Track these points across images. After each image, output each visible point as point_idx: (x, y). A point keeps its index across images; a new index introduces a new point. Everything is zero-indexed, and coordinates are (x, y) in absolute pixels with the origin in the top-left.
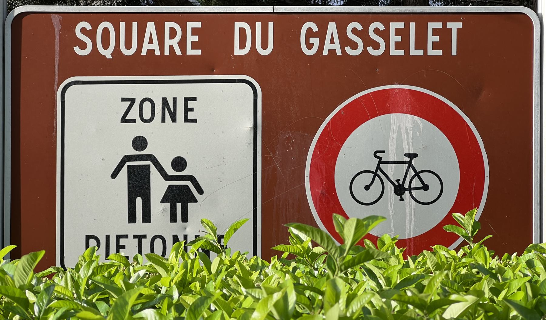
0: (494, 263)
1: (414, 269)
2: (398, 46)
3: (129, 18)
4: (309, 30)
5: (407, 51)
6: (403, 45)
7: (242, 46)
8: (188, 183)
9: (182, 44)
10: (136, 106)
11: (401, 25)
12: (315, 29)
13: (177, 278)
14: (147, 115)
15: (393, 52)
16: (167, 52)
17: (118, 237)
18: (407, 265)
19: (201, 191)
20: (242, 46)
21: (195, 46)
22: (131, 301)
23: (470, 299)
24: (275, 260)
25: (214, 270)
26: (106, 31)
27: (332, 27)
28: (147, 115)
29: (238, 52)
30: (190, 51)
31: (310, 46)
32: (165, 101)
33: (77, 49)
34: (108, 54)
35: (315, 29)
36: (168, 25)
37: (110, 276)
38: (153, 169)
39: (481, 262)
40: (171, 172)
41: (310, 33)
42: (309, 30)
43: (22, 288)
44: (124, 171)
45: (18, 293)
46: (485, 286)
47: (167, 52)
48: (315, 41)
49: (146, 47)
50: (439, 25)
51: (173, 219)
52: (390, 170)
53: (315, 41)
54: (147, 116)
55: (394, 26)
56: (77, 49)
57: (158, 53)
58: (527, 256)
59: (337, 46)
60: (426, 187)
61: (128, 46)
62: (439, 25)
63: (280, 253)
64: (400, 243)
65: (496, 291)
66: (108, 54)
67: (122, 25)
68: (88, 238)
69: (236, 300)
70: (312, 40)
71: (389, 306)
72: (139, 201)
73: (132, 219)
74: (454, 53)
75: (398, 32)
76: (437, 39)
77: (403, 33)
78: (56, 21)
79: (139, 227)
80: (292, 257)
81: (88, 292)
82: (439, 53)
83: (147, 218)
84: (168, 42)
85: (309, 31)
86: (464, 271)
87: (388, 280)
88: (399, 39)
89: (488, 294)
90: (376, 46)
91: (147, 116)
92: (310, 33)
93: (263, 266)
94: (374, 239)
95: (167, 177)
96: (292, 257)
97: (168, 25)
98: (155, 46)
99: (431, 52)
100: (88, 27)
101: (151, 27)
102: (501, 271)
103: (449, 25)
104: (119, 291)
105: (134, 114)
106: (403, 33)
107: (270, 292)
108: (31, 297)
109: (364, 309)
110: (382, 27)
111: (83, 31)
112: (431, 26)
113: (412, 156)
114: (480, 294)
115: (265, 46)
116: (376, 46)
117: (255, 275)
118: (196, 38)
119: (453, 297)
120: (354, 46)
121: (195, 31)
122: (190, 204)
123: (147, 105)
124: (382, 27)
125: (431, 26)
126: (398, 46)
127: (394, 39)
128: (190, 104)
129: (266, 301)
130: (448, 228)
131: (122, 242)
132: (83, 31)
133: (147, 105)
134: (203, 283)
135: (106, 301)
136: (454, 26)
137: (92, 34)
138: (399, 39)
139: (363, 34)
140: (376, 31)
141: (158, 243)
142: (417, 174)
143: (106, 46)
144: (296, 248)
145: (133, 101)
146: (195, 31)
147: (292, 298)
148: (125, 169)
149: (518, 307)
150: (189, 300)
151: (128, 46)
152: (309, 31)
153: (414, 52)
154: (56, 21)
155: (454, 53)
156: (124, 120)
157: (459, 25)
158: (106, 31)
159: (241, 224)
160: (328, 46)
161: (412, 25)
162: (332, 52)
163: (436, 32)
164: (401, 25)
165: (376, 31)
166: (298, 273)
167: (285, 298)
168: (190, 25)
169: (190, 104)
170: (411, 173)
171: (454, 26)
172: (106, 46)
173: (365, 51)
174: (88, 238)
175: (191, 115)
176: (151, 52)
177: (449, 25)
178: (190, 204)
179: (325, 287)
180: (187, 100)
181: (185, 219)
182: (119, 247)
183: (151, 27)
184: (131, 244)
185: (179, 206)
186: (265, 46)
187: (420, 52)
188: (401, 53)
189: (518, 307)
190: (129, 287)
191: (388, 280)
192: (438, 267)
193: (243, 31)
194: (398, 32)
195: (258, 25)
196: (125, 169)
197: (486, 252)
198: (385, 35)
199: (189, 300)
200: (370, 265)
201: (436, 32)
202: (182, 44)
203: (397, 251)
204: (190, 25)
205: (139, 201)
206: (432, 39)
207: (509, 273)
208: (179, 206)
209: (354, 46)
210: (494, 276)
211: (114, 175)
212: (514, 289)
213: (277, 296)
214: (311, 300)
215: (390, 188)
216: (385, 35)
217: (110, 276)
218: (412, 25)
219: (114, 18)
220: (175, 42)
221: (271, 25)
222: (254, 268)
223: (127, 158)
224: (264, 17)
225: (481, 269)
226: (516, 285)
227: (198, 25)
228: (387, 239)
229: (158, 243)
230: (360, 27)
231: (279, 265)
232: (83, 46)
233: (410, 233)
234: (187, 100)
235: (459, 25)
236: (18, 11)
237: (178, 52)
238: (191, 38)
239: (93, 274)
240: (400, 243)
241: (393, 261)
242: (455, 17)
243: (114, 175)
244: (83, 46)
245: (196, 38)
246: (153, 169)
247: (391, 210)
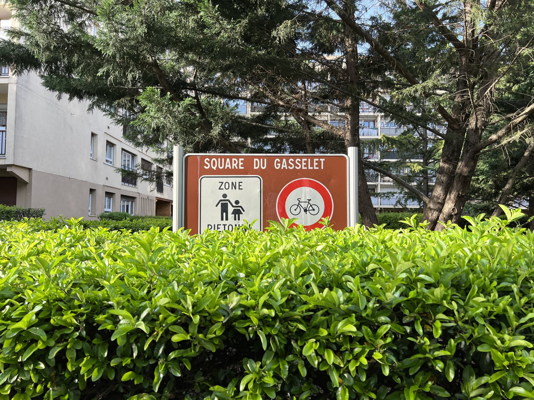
0: (334, 233)
1: (309, 235)
2: (305, 166)
3: (221, 157)
4: (277, 161)
5: (308, 168)
6: (306, 166)
7: (257, 166)
8: (240, 208)
9: (238, 165)
10: (224, 184)
11: (306, 160)
12: (279, 161)
13: (234, 238)
14: (227, 187)
15: (303, 168)
16: (233, 168)
17: (218, 225)
18: (306, 234)
19: (244, 211)
20: (257, 166)
21: (242, 166)
22: (218, 245)
23: (324, 244)
24: (266, 232)
25: (246, 235)
26: (214, 161)
27: (284, 160)
28: (227, 187)
29: (255, 168)
30: (240, 168)
31: (277, 166)
32: (232, 183)
33: (205, 167)
34: (215, 168)
35: (279, 161)
36: (233, 159)
37: (214, 237)
38: (229, 204)
39: (329, 233)
40: (235, 205)
41: (277, 162)
42: (277, 161)
43: (184, 240)
44: (220, 204)
45: (183, 242)
46: (330, 240)
47: (233, 168)
48: (279, 165)
49: (227, 166)
50: (317, 160)
51: (235, 219)
52: (302, 204)
53: (279, 165)
54: (227, 188)
55: (303, 160)
56: (205, 167)
57: (230, 168)
58: (345, 231)
59: (286, 166)
60: (314, 210)
61: (221, 166)
62: (317, 160)
63: (267, 230)
64: (305, 227)
65: (333, 242)
66: (215, 168)
67: (219, 159)
68: (208, 225)
69: (252, 244)
70: (278, 164)
71: (299, 246)
72: (224, 214)
73: (222, 219)
74: (322, 168)
75: (305, 162)
76: (317, 164)
77: (306, 162)
78: (199, 158)
79: (224, 222)
80: (271, 231)
81: (206, 242)
82: (318, 168)
83: (227, 219)
84: (233, 165)
85: (277, 161)
86: (324, 236)
87: (300, 238)
88: (305, 164)
89: (331, 243)
90: (298, 166)
91: (227, 188)
92: (277, 162)
93: (262, 234)
94: (296, 225)
95: (233, 206)
96: (271, 231)
97: (233, 159)
98: (229, 166)
99: (315, 168)
100: (209, 160)
101: (228, 160)
102: (335, 236)
103: (321, 160)
104: (215, 241)
105: (223, 187)
106: (306, 162)
107: (261, 242)
108: (187, 243)
109: (292, 247)
110: (300, 160)
111: (207, 161)
112: (315, 160)
113: (310, 200)
114: (328, 243)
115: (263, 166)
116: (298, 166)
117: (259, 237)
118: (242, 164)
119: (319, 244)
120: (291, 166)
121: (242, 161)
122: (240, 215)
123: (227, 184)
124: (300, 160)
125: (315, 160)
126: (305, 166)
127: (304, 164)
128: (241, 184)
129: (260, 245)
130: (320, 222)
131: (219, 226)
132: (207, 161)
133: (227, 184)
134: (242, 239)
135: (212, 245)
136: (322, 160)
137: (210, 162)
138: (305, 164)
139: (294, 162)
140: (298, 161)
141: (230, 227)
142: (311, 206)
143: (214, 166)
144: (272, 228)
145: (222, 183)
146: (242, 161)
147: (269, 244)
148: (220, 204)
149: (340, 247)
150: (237, 244)
151: (221, 166)
152: (277, 161)
153: (310, 168)
154: (199, 158)
155: (322, 168)
156: (220, 189)
157: (324, 160)
158: (214, 161)
159: (255, 221)
160: (283, 166)
161: (309, 160)
162: (284, 168)
163: (316, 162)
164: (306, 160)
165: (298, 161)
166: (272, 236)
167: (266, 244)
168: (240, 160)
169: (241, 184)
170: (309, 205)
171: (322, 160)
172: (214, 166)
173: (295, 168)
174: (208, 225)
175: (241, 187)
176: (228, 168)
177: (321, 160)
178: (240, 215)
179: (279, 241)
180: (239, 183)
181: (239, 219)
182: (218, 228)
183: (228, 160)
184: (222, 227)
185: (237, 215)
186: (263, 166)
187: (312, 168)
188: (306, 168)
189: (340, 247)
190: (218, 240)
191: (300, 238)
192: (316, 234)
193: (257, 161)
194: (305, 162)
195: (261, 160)
196: (220, 204)
197: (13, 123)
198: (301, 163)
199: (237, 244)
200: (295, 233)
201: (316, 162)
202: (238, 165)
203: (303, 229)
204: (240, 160)
205: (224, 214)
206: (315, 164)
207: (338, 236)
208: (237, 215)
209: (291, 166)
210: (333, 237)
211: (217, 206)
212: (339, 241)
213: (264, 243)
214: (275, 245)
215: (302, 210)
216: (301, 163)
217: (214, 237)
218: (309, 160)
219: (217, 157)
220: (236, 165)
221: (265, 160)
222: (259, 234)
223: (221, 200)
224: (263, 157)
225: (329, 235)
226: (340, 240)
227: (243, 159)
228: (300, 226)
229: (230, 227)
230: (293, 160)
231: (267, 234)
232: (207, 166)
233: (309, 224)
234: (239, 183)
235: (324, 160)
236: (187, 155)
237: (237, 168)
238: (241, 164)
239: (208, 236)
240: (305, 227)
241: (302, 232)
242: (322, 157)
243: (217, 206)
244: (207, 166)
245: (242, 164)
246: (229, 204)
247: (303, 217)
